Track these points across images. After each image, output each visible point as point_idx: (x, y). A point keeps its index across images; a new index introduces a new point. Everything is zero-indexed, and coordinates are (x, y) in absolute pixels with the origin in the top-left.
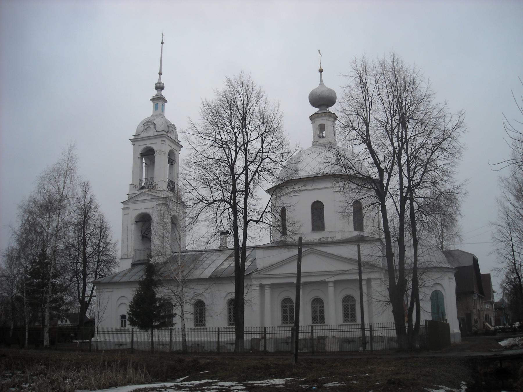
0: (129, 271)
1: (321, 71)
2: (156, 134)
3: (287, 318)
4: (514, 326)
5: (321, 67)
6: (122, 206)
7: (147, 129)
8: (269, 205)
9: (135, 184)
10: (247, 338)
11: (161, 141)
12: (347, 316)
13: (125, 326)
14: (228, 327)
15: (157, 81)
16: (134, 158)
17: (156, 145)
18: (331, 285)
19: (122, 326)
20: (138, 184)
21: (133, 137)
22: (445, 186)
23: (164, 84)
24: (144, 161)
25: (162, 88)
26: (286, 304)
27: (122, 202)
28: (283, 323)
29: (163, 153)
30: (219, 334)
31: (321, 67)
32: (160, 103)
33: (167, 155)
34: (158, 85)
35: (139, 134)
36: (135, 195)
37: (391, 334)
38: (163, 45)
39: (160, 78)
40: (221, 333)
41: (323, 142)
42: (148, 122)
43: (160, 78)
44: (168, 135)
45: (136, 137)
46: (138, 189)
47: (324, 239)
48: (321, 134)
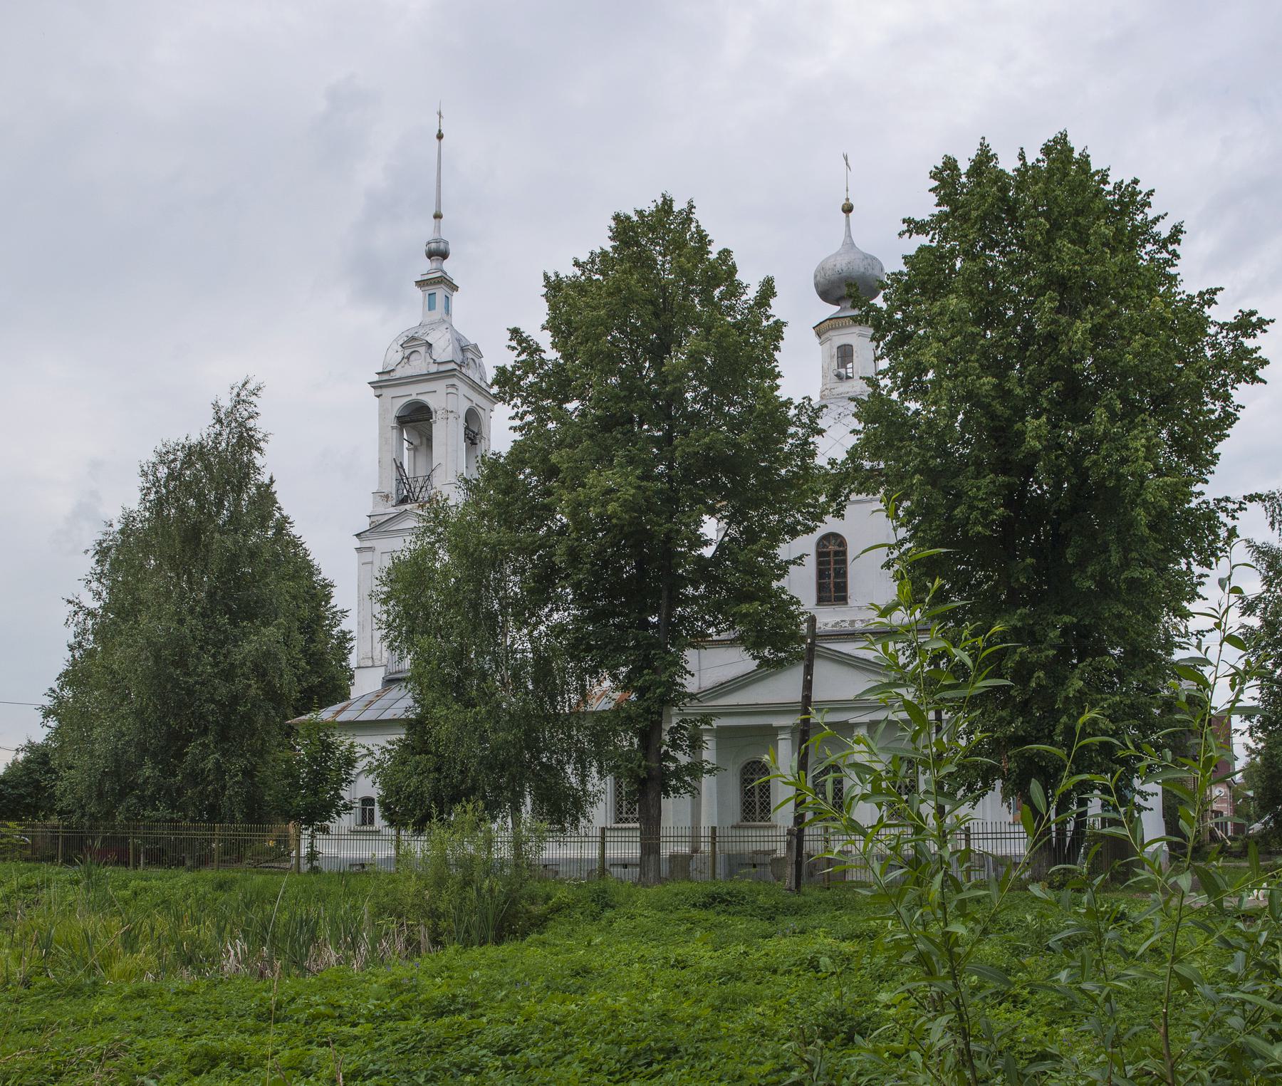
0: (378, 696)
1: (848, 209)
2: (434, 368)
3: (754, 807)
4: (913, 613)
5: (847, 199)
6: (357, 543)
7: (412, 358)
8: (370, 664)
9: (386, 491)
10: (666, 850)
11: (448, 386)
12: (750, 811)
13: (372, 822)
14: (614, 825)
15: (844, 202)
16: (381, 428)
17: (437, 398)
18: (861, 732)
19: (364, 823)
20: (394, 492)
21: (376, 378)
22: (154, 459)
23: (447, 243)
24: (405, 437)
25: (444, 255)
26: (752, 774)
27: (358, 535)
28: (745, 819)
29: (451, 416)
30: (603, 844)
31: (847, 199)
32: (440, 292)
33: (462, 421)
34: (433, 246)
35: (393, 370)
36: (386, 518)
37: (999, 849)
38: (442, 140)
39: (438, 229)
40: (608, 839)
41: (847, 390)
42: (413, 339)
43: (438, 229)
44: (464, 370)
45: (385, 377)
46: (394, 503)
47: (847, 625)
48: (843, 371)
